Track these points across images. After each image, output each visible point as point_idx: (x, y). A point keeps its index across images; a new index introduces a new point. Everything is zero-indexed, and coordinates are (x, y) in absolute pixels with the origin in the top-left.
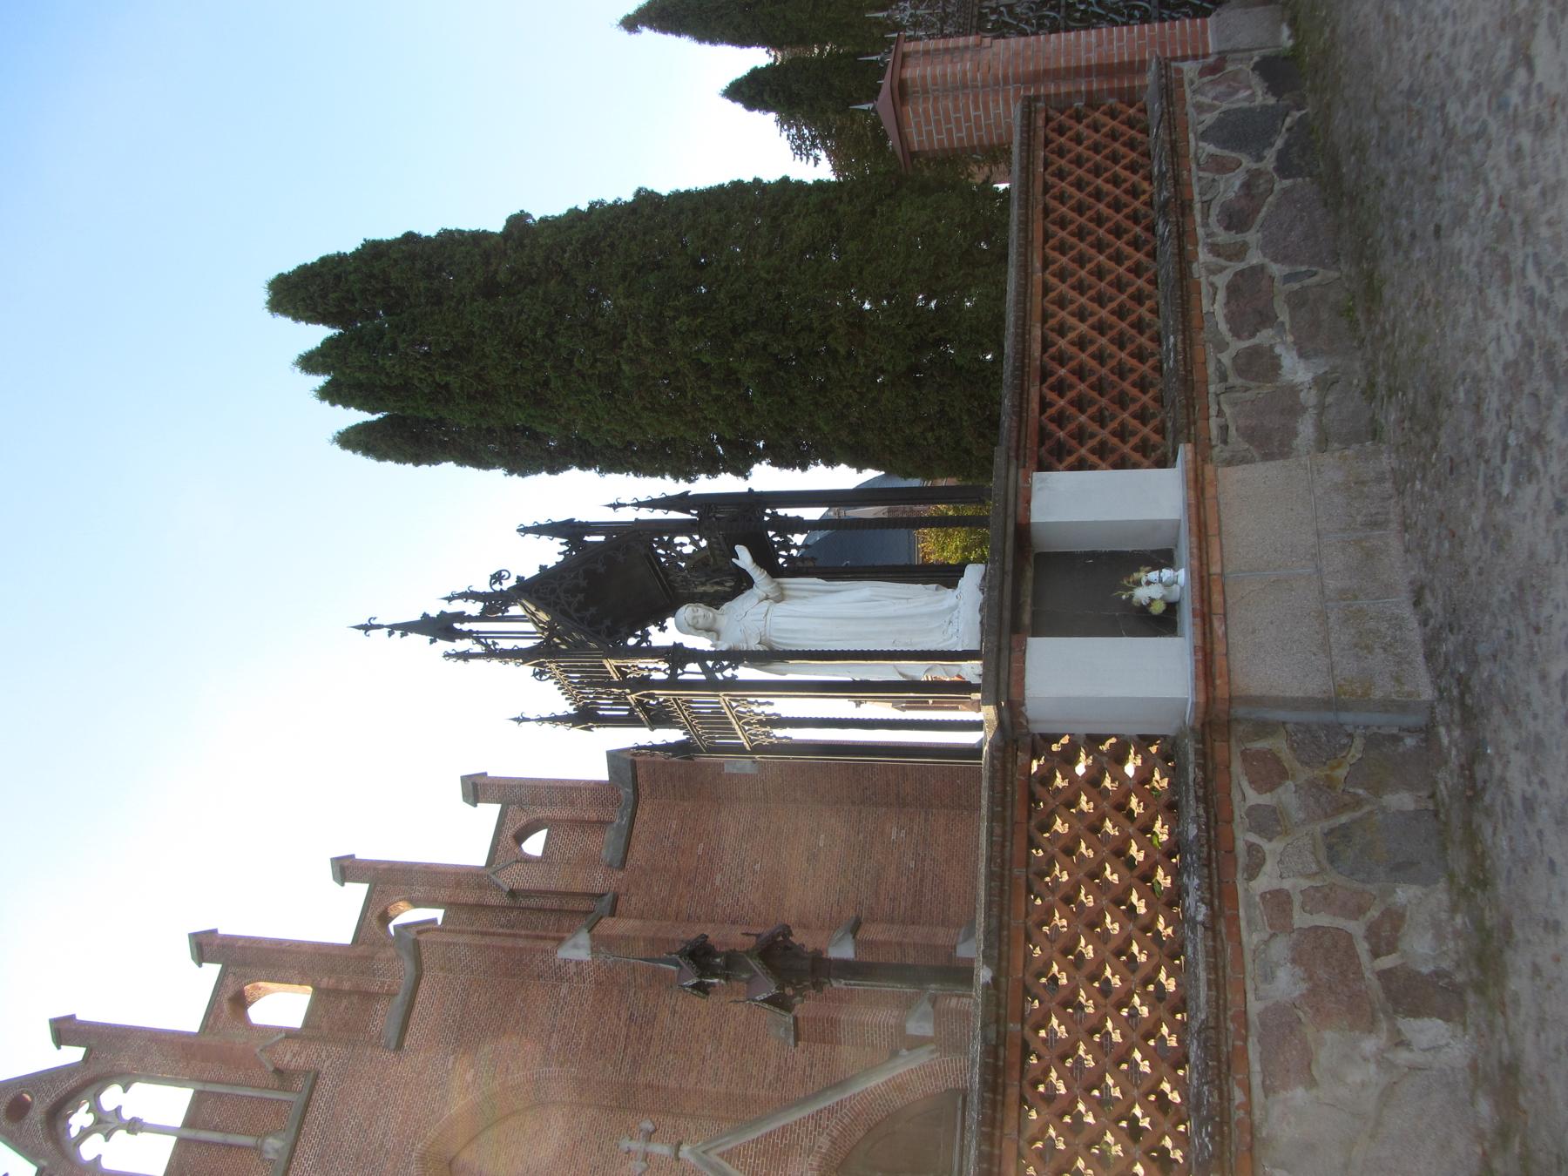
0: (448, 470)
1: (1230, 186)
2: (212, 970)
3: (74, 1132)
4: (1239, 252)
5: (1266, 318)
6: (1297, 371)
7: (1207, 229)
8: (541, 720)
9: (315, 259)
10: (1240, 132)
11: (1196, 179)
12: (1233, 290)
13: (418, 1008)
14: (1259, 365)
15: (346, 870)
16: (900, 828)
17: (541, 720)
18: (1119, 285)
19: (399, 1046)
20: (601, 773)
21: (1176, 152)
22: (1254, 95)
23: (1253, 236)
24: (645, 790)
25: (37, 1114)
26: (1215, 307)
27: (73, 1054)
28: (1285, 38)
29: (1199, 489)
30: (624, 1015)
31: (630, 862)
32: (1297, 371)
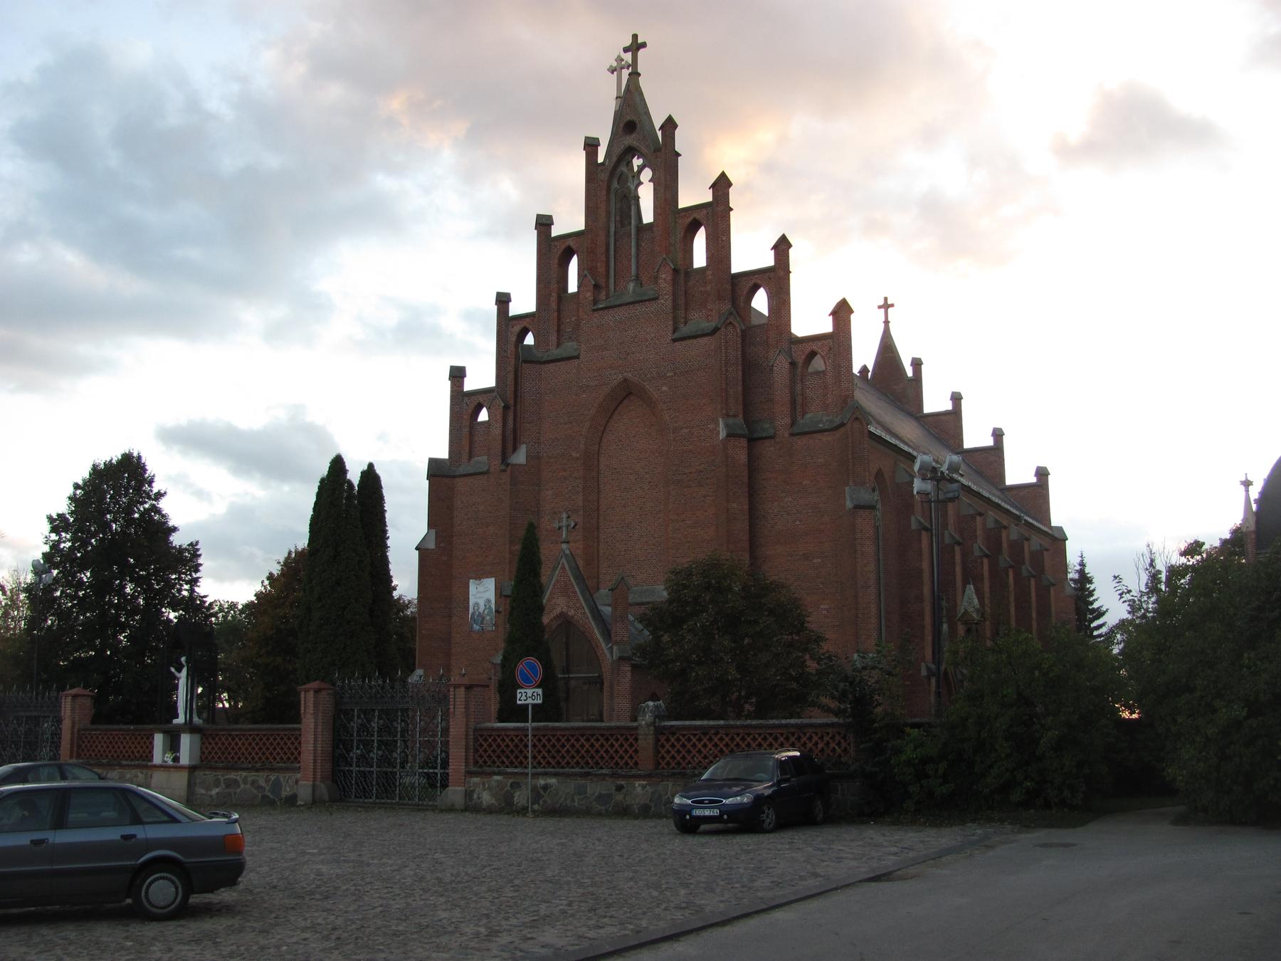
0: (314, 499)
1: (262, 783)
3: (636, 169)
4: (245, 783)
5: (228, 786)
6: (214, 792)
7: (252, 775)
8: (887, 322)
10: (276, 786)
12: (236, 781)
13: (695, 341)
14: (217, 783)
16: (828, 610)
17: (887, 322)
18: (626, 751)
19: (674, 340)
20: (254, 598)
21: (272, 770)
22: (286, 792)
23: (248, 786)
25: (630, 140)
26: (233, 775)
27: (910, 373)
29: (183, 767)
31: (795, 438)
32: (214, 792)
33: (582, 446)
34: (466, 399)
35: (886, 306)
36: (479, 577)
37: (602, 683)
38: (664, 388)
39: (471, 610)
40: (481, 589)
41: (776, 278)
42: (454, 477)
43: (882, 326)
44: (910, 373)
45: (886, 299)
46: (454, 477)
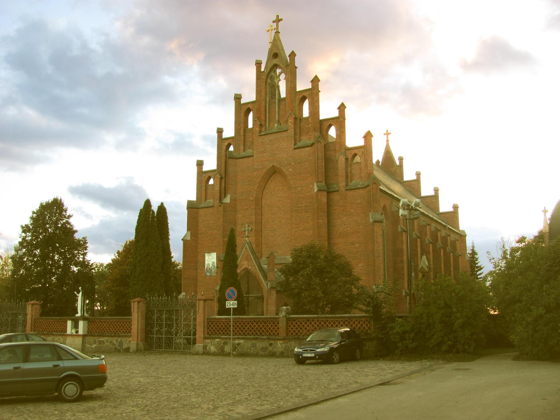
1: (115, 342)
2: (452, 210)
3: (278, 74)
4: (107, 342)
5: (100, 344)
6: (94, 346)
7: (110, 339)
8: (388, 141)
9: (196, 167)
10: (121, 344)
11: (116, 338)
12: (103, 341)
13: (304, 149)
15: (418, 174)
16: (362, 267)
17: (388, 141)
18: (274, 328)
20: (111, 262)
21: (119, 336)
22: (125, 346)
23: (108, 344)
24: (366, 190)
26: (102, 339)
28: (131, 351)
30: (306, 204)
31: (347, 192)
32: (94, 346)
33: (254, 195)
34: (204, 175)
35: (387, 134)
36: (209, 252)
37: (263, 299)
38: (290, 170)
39: (206, 267)
40: (210, 257)
41: (339, 121)
42: (199, 208)
43: (385, 143)
44: (398, 163)
45: (387, 131)
46: (199, 208)
